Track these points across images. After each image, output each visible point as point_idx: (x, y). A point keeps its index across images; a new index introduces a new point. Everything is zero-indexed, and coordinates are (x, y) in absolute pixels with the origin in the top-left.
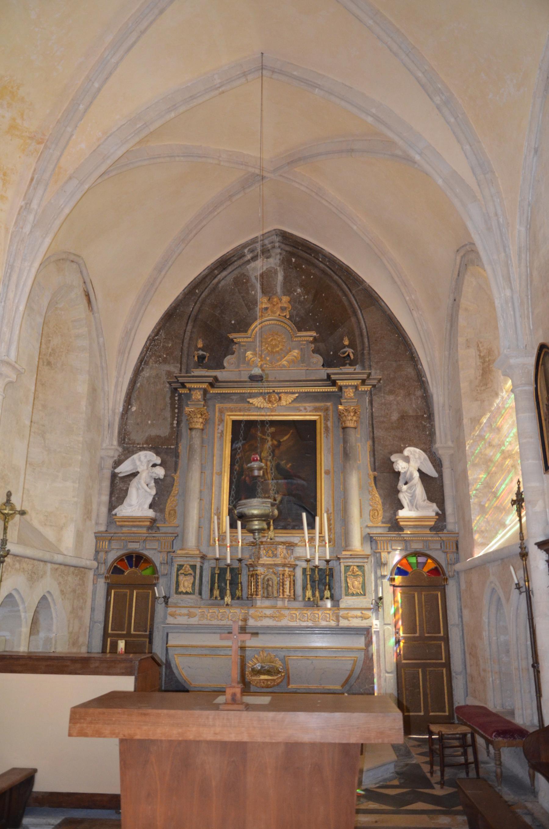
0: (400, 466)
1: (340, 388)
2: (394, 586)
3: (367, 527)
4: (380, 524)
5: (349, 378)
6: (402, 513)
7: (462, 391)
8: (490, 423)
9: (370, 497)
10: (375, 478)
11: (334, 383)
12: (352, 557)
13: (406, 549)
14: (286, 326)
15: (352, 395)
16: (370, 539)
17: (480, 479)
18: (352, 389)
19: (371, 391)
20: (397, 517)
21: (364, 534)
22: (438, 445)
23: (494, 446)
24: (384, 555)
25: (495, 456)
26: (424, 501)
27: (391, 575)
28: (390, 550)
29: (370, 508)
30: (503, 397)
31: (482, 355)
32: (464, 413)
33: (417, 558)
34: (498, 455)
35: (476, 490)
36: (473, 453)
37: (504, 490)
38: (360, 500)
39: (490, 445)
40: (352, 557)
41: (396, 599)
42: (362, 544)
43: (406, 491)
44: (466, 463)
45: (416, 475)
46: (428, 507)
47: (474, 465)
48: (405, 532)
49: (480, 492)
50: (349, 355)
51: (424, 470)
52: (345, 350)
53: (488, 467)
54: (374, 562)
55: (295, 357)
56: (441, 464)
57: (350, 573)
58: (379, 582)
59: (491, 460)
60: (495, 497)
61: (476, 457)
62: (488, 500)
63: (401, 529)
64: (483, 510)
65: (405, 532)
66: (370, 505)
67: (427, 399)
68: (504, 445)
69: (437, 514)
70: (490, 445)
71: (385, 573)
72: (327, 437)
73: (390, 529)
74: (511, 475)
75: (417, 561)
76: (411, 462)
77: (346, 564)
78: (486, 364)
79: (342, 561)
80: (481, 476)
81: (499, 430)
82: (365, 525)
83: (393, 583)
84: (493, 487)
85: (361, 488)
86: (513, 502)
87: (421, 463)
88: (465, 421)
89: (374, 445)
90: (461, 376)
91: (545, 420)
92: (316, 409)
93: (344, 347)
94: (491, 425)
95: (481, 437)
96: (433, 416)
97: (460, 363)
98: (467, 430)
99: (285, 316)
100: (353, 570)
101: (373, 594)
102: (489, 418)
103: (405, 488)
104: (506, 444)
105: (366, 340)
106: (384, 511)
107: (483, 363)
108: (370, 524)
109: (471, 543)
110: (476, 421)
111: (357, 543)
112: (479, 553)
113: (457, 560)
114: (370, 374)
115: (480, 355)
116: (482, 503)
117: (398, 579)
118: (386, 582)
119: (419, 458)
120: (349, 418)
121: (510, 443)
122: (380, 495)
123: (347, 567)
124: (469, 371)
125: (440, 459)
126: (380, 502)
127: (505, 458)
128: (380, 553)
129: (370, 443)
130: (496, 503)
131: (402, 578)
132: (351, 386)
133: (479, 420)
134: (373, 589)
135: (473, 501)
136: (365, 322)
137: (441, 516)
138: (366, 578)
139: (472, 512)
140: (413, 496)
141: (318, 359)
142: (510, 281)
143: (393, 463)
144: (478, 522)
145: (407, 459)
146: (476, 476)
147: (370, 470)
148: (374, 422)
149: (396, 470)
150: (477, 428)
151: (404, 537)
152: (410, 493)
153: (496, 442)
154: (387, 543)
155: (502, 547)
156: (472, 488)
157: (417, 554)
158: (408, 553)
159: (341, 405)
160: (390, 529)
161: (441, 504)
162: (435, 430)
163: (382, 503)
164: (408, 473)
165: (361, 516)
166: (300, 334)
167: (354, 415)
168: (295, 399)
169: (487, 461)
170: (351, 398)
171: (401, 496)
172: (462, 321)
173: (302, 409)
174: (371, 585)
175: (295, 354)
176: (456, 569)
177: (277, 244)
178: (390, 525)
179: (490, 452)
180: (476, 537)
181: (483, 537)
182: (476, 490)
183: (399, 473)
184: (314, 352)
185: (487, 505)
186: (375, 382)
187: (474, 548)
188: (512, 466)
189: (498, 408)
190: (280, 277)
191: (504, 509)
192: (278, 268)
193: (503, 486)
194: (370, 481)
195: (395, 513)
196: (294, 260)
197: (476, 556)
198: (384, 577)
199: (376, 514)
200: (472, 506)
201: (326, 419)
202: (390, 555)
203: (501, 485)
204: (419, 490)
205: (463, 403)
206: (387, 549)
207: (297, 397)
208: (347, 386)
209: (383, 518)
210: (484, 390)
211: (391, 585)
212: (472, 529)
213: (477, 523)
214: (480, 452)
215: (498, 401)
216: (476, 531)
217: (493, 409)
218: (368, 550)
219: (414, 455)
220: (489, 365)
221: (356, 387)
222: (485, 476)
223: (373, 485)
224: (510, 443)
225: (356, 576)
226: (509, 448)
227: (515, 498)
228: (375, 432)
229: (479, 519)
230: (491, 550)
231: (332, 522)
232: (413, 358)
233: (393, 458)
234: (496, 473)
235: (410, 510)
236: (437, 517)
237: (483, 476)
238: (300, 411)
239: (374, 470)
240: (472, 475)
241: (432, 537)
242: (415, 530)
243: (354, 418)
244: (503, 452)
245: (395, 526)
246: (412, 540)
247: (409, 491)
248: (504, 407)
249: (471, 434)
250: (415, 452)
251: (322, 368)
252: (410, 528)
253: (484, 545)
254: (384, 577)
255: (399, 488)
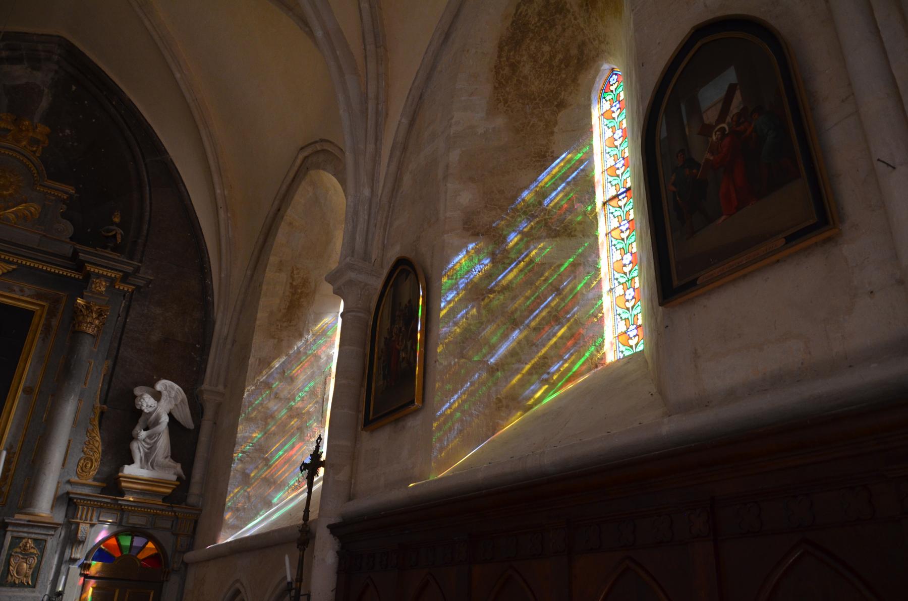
0: (147, 402)
1: (88, 276)
2: (86, 577)
3: (69, 482)
4: (90, 482)
5: (105, 273)
6: (130, 470)
7: (258, 322)
8: (282, 371)
9: (87, 439)
10: (102, 413)
11: (80, 266)
12: (31, 525)
13: (118, 523)
14: (31, 165)
15: (103, 289)
16: (67, 502)
17: (252, 438)
18: (106, 281)
19: (132, 292)
20: (120, 474)
21: (60, 492)
22: (205, 386)
23: (281, 399)
24: (82, 527)
25: (280, 412)
26: (166, 457)
27: (86, 559)
28: (95, 521)
29: (82, 455)
30: (307, 341)
31: (294, 283)
32: (253, 350)
33: (132, 539)
34: (284, 411)
35: (243, 452)
36: (251, 404)
37: (280, 457)
38: (69, 441)
39: (277, 396)
40: (31, 525)
41: (84, 596)
42: (53, 507)
43: (144, 440)
44: (239, 415)
45: (165, 419)
46: (169, 467)
47: (249, 419)
48: (125, 498)
49: (248, 456)
50: (115, 236)
51: (176, 415)
52: (111, 227)
53: (267, 424)
54: (65, 537)
55: (31, 213)
56: (202, 414)
57: (19, 550)
58: (64, 568)
59: (272, 417)
60: (266, 465)
61: (254, 409)
62: (257, 467)
63: (121, 493)
64: (246, 479)
65: (125, 498)
66: (83, 451)
67: (206, 325)
68: (294, 400)
69: (179, 479)
70: (277, 396)
71: (78, 556)
72: (43, 340)
73: (103, 491)
74: (294, 440)
75: (132, 542)
76: (162, 401)
77: (16, 534)
78: (297, 296)
79: (10, 528)
80: (254, 435)
81: (292, 379)
82: (67, 478)
83: (86, 572)
84: (267, 452)
85: (75, 423)
86: (304, 466)
87: (176, 405)
88: (252, 360)
89: (114, 368)
90: (261, 303)
91: (379, 359)
92: (39, 296)
93: (113, 223)
94: (284, 372)
95: (268, 385)
96: (209, 349)
97: (264, 287)
98: (250, 373)
99: (34, 152)
100: (26, 546)
101: (49, 586)
102: (284, 362)
103: (143, 434)
104: (298, 399)
105: (145, 227)
106: (102, 463)
107: (293, 294)
108: (75, 479)
109: (218, 524)
110: (266, 363)
111: (44, 505)
112: (227, 538)
113: (190, 547)
114: (137, 270)
115: (291, 284)
116: (247, 471)
117: (96, 566)
118: (75, 569)
119: (175, 398)
120: (89, 320)
121: (302, 399)
122: (102, 439)
123: (16, 540)
124: (270, 301)
125: (201, 405)
126: (100, 449)
127: (291, 417)
128: (78, 524)
129: (110, 363)
130: (266, 473)
131: (102, 566)
132: (106, 276)
133: (269, 363)
134: (51, 578)
135: (236, 466)
136: (151, 203)
137: (184, 483)
138: (44, 559)
139: (230, 481)
140: (152, 449)
141: (68, 229)
142: (373, 180)
143: (135, 397)
144: (234, 494)
145: (157, 396)
146: (247, 434)
147: (98, 401)
148: (124, 337)
149: (138, 407)
150: (264, 372)
151: (121, 505)
152: (148, 444)
153: (284, 394)
154: (93, 511)
155: (264, 531)
156: (238, 448)
157: (133, 532)
158: (120, 529)
159: (82, 298)
160: (103, 491)
161: (188, 468)
162: (206, 367)
163: (103, 451)
164: (154, 415)
165: (63, 465)
166: (50, 183)
167: (97, 318)
168: (9, 272)
169: (268, 417)
170: (100, 293)
171: (135, 446)
172: (281, 236)
173: (15, 288)
174: (49, 573)
175: (33, 209)
176: (185, 560)
177: (56, 58)
178: (105, 485)
179: (273, 405)
180: (228, 516)
181: (237, 518)
182: (243, 452)
183: (141, 412)
184: (63, 215)
185: (252, 475)
186: (141, 283)
187: (220, 530)
188: (298, 429)
189: (299, 352)
190: (44, 103)
191: (275, 482)
192: (46, 90)
193: (281, 453)
194: (92, 416)
195: (119, 468)
196: (74, 88)
197: (221, 541)
198: (73, 561)
199: (89, 466)
200: (232, 473)
201: (52, 313)
202: (94, 528)
203: (278, 450)
204: (163, 442)
205: (255, 337)
206: (91, 520)
207: (14, 269)
208: (99, 276)
209: (98, 473)
210: (286, 327)
211: (81, 575)
212: (224, 505)
213: (233, 498)
214: (261, 404)
215: (300, 344)
216: (229, 508)
217: (291, 352)
218: (59, 517)
219: (170, 392)
220: (300, 298)
221: (112, 281)
222: (259, 436)
223: (96, 423)
224: (302, 399)
225: (26, 555)
226: (300, 405)
227: (308, 461)
228: (122, 349)
229: (238, 492)
230: (247, 535)
231: (13, 467)
232: (203, 269)
233: (137, 391)
234: (274, 434)
235: (142, 468)
236: (178, 483)
237: (257, 435)
238: (13, 291)
239: (104, 401)
240: (242, 430)
241: (162, 510)
242: (141, 497)
243: (97, 322)
244: (291, 409)
245: (112, 485)
246: (133, 511)
247: (148, 441)
248: (306, 353)
249: (254, 378)
250: (172, 388)
251: (68, 240)
252: (135, 493)
253: (238, 528)
254: (73, 561)
255: (134, 433)
